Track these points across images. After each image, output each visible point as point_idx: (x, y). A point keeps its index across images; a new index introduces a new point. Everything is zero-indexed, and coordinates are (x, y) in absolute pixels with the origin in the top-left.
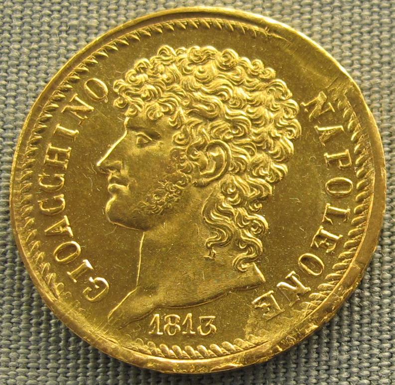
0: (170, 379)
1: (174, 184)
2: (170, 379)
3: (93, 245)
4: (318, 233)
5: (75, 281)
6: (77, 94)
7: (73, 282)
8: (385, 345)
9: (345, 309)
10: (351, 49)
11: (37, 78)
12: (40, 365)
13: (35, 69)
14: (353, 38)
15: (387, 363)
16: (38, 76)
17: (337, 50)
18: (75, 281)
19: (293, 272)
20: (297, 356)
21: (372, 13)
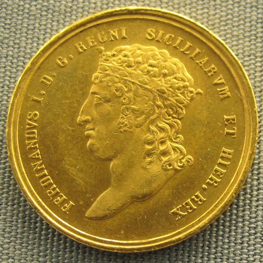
0: (105, 253)
1: (74, 111)
2: (105, 253)
3: (79, 194)
4: (215, 169)
5: (68, 213)
6: (190, 199)
7: (67, 213)
8: (237, 258)
9: (228, 211)
10: (250, 22)
11: (4, 80)
12: (22, 258)
13: (253, 247)
14: (250, 64)
15: (256, 177)
16: (5, 79)
17: (241, 56)
18: (68, 213)
19: (199, 192)
20: (211, 231)
21: (243, 217)
